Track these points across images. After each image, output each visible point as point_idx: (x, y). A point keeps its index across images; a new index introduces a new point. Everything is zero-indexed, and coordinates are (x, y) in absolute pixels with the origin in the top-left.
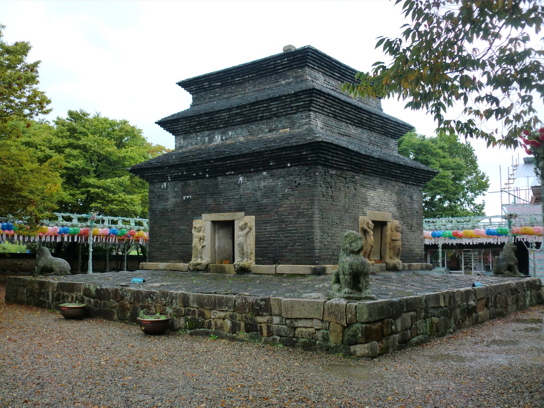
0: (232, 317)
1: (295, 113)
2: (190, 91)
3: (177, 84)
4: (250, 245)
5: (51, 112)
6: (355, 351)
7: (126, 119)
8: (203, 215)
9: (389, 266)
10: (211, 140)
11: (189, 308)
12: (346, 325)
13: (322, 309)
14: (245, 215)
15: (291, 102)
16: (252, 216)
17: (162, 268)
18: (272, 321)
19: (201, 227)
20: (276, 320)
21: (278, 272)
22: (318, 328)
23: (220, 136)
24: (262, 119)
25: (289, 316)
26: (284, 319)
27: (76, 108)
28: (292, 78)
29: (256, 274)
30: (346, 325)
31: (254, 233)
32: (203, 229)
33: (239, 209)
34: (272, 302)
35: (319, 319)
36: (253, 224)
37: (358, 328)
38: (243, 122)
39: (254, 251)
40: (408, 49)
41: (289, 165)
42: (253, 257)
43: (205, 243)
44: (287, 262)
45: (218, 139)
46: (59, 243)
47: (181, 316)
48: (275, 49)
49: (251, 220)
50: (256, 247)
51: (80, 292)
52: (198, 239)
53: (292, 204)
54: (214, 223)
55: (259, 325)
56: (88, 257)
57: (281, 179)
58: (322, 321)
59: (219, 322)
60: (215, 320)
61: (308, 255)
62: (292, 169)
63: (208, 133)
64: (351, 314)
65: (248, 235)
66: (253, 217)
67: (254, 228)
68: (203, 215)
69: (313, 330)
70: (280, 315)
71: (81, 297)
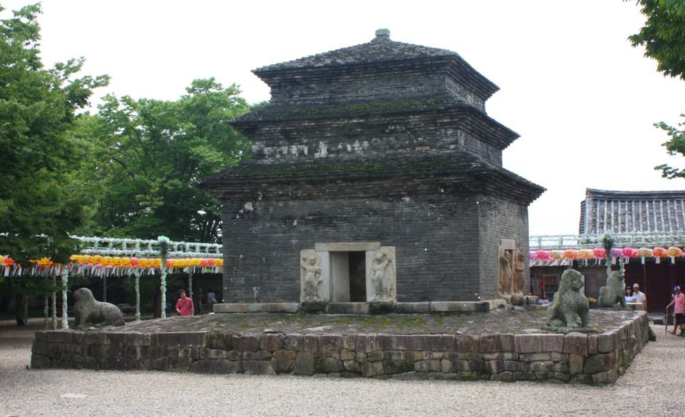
0: (452, 358)
2: (269, 83)
3: (252, 71)
4: (391, 281)
5: (657, 122)
8: (316, 244)
9: (515, 300)
10: (313, 151)
11: (392, 351)
12: (587, 356)
13: (562, 342)
14: (381, 245)
16: (391, 247)
17: (253, 310)
18: (503, 357)
19: (315, 259)
20: (508, 356)
22: (556, 360)
25: (522, 351)
27: (191, 82)
30: (587, 356)
31: (395, 267)
32: (318, 261)
33: (370, 239)
34: (501, 339)
35: (559, 352)
37: (601, 358)
39: (395, 287)
40: (439, 79)
42: (394, 294)
43: (321, 278)
46: (6, 277)
47: (379, 361)
49: (390, 251)
50: (397, 282)
51: (201, 343)
52: (313, 274)
53: (447, 234)
54: (331, 253)
55: (487, 362)
56: (160, 293)
58: (562, 353)
61: (467, 291)
64: (593, 345)
65: (387, 268)
66: (393, 248)
67: (394, 262)
68: (316, 244)
69: (551, 362)
71: (205, 350)
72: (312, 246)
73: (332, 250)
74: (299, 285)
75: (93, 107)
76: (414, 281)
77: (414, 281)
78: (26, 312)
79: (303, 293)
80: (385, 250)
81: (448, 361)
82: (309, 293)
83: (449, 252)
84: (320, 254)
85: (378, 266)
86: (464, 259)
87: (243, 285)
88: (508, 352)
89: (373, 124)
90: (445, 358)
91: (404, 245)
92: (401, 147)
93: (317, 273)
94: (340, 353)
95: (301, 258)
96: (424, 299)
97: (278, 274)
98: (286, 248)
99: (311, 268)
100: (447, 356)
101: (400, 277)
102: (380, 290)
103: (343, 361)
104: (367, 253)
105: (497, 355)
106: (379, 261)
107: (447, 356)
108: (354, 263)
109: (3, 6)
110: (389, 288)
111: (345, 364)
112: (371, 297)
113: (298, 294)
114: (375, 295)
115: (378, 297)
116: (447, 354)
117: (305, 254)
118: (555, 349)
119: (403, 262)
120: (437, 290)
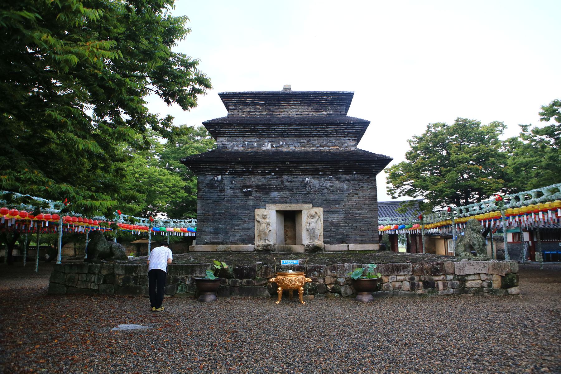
1: (344, 137)
6: (511, 292)
7: (553, 100)
15: (346, 129)
21: (350, 249)
23: (270, 144)
24: (315, 136)
26: (456, 277)
28: (330, 112)
29: (329, 251)
31: (322, 221)
32: (268, 216)
36: (322, 213)
38: (296, 136)
41: (354, 173)
42: (322, 239)
43: (271, 228)
44: (355, 241)
45: (268, 146)
48: (278, 87)
49: (320, 211)
57: (346, 182)
59: (397, 285)
60: (393, 283)
62: (356, 175)
63: (256, 139)
66: (321, 209)
70: (453, 273)
72: (264, 206)
73: (278, 209)
74: (254, 233)
75: (144, 105)
76: (335, 230)
77: (335, 230)
78: (6, 259)
79: (256, 238)
80: (316, 209)
81: (408, 283)
82: (506, 217)
83: (358, 212)
84: (269, 212)
85: (312, 220)
86: (369, 216)
87: (211, 233)
88: (450, 274)
89: (302, 129)
90: (406, 280)
91: (329, 206)
92: (320, 146)
93: (268, 224)
94: (324, 279)
95: (256, 214)
96: (342, 242)
97: (238, 225)
98: (245, 207)
99: (264, 221)
100: (407, 279)
101: (326, 228)
102: (313, 236)
103: (326, 285)
104: (303, 212)
105: (442, 277)
106: (313, 217)
107: (407, 279)
108: (290, 219)
109: (175, 3)
110: (319, 235)
111: (329, 287)
112: (306, 241)
113: (253, 239)
114: (309, 239)
115: (311, 241)
116: (407, 278)
117: (259, 212)
118: (483, 272)
119: (328, 218)
120: (351, 236)
